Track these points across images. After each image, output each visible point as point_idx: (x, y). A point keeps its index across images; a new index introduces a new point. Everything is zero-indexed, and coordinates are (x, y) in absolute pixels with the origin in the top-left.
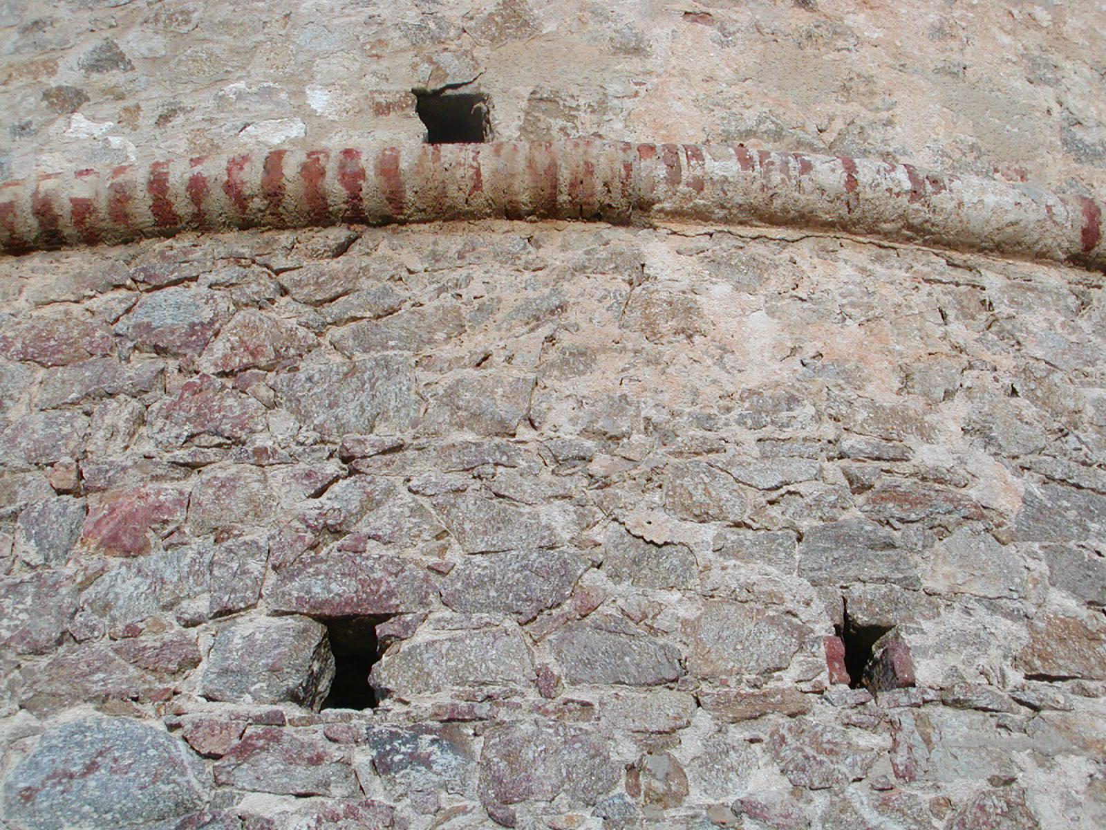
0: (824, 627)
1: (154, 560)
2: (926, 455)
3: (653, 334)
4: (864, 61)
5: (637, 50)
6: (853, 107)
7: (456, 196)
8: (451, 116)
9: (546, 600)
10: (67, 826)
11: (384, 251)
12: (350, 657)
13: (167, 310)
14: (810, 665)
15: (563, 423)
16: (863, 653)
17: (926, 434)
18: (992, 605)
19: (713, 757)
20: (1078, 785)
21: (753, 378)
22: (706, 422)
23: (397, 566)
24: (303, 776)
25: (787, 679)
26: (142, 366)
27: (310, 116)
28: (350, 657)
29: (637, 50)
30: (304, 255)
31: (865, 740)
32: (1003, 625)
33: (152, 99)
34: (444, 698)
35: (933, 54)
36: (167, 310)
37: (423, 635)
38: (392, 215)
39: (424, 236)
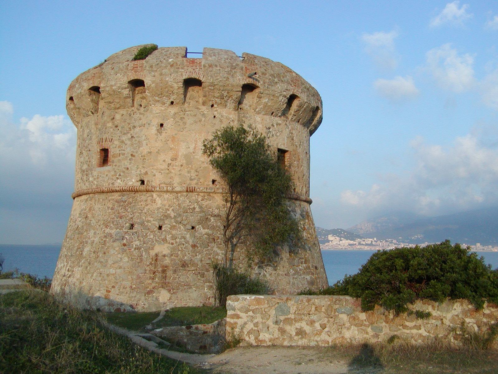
0: (158, 226)
1: (122, 219)
2: (168, 212)
3: (152, 202)
4: (172, 175)
5: (155, 176)
6: (171, 180)
7: (141, 190)
8: (143, 182)
9: (142, 224)
10: (1, 337)
11: (138, 195)
12: (132, 226)
13: (125, 198)
14: (156, 229)
15: (145, 211)
16: (160, 228)
17: (169, 211)
18: (169, 224)
19: (150, 235)
20: (170, 237)
21: (158, 206)
22: (154, 210)
23: (135, 221)
24: (129, 235)
25: (155, 230)
26: (122, 203)
27: (133, 182)
28: (132, 226)
29: (155, 176)
30: (132, 194)
31: (158, 234)
32: (169, 226)
33: (123, 179)
34: (136, 231)
35: (179, 173)
36: (125, 198)
37: (136, 226)
38: (136, 191)
39: (140, 193)
